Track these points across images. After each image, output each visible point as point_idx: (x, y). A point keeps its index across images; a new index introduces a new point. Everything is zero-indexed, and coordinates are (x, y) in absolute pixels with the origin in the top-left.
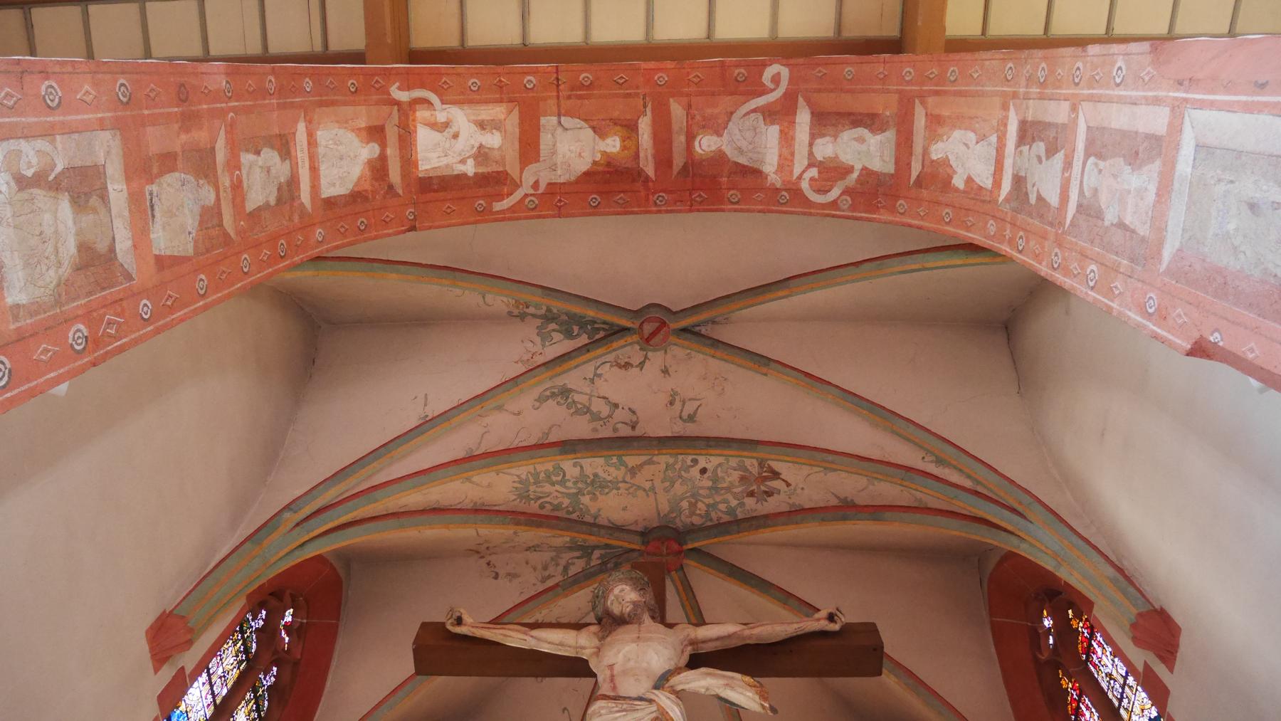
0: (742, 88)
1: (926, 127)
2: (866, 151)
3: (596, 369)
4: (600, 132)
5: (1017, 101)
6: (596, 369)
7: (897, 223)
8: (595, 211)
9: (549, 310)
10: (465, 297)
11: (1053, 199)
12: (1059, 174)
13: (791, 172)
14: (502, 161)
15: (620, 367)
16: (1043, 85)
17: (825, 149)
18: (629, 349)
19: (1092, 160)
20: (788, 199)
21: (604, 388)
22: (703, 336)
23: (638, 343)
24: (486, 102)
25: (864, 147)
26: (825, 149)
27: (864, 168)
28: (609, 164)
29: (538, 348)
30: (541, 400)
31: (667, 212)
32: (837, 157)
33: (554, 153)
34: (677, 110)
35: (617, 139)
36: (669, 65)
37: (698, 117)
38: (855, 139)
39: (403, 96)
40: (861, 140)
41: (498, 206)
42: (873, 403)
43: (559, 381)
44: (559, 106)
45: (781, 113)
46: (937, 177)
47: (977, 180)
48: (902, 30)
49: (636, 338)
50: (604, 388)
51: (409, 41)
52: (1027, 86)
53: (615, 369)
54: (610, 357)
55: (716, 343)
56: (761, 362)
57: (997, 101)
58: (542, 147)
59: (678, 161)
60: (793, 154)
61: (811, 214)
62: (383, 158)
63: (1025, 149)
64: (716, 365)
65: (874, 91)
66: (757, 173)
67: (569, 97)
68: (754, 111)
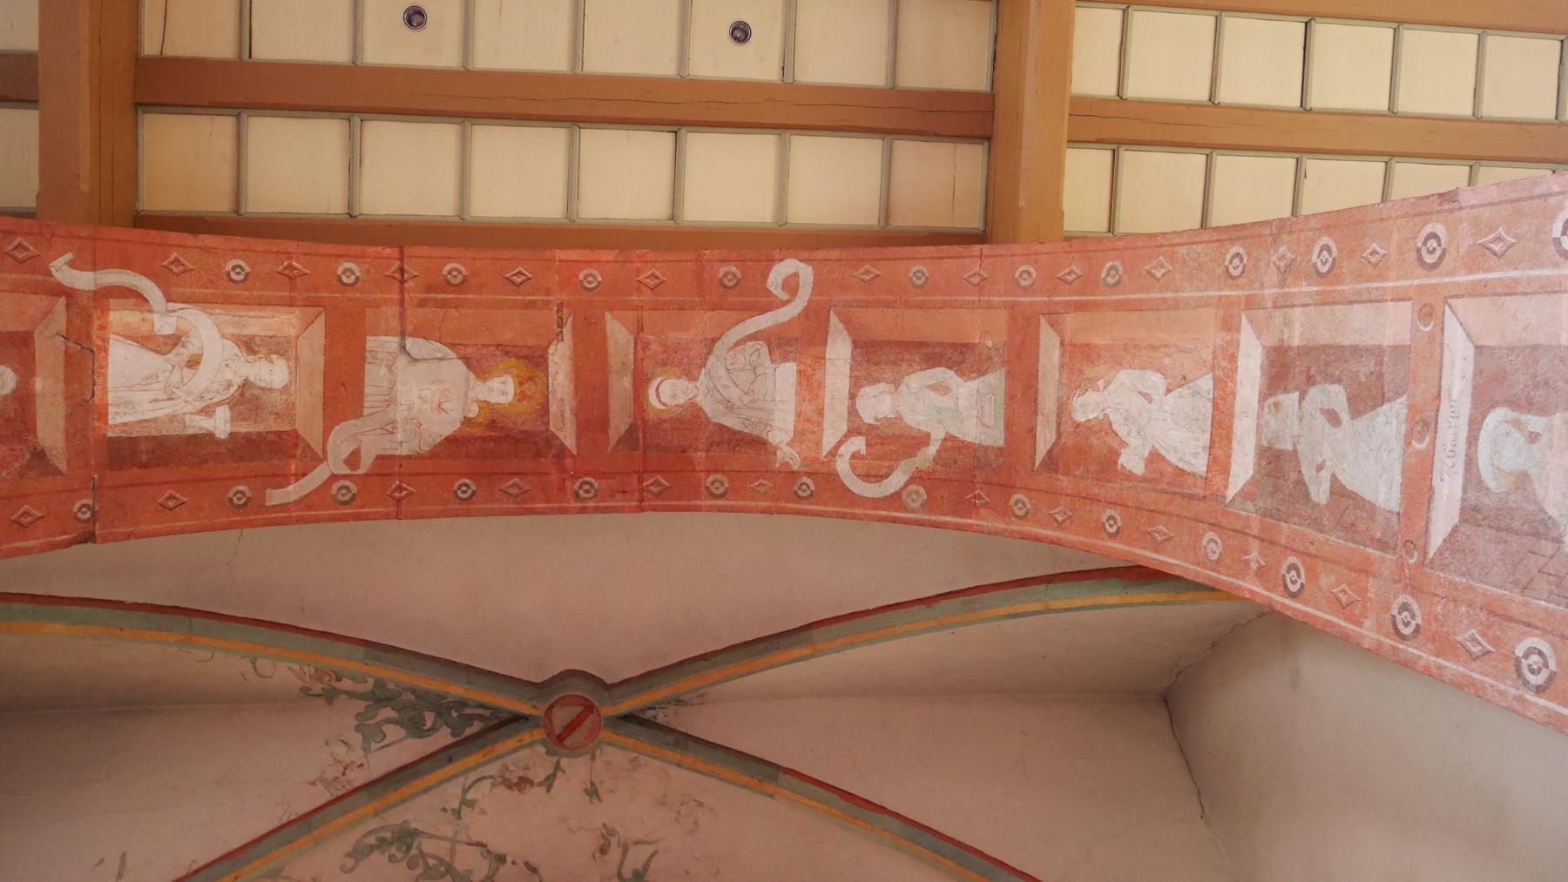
0: (732, 299)
1: (1062, 366)
2: (951, 408)
3: (465, 791)
4: (478, 367)
5: (1260, 314)
6: (465, 791)
7: (1012, 534)
8: (466, 508)
9: (380, 684)
10: (218, 662)
11: (1385, 493)
12: (1397, 446)
13: (819, 443)
14: (289, 412)
15: (510, 786)
16: (1331, 276)
17: (877, 403)
18: (526, 754)
19: (1496, 418)
20: (812, 490)
21: (478, 826)
22: (661, 727)
23: (543, 742)
24: (262, 303)
25: (947, 401)
26: (877, 403)
27: (949, 438)
28: (492, 424)
29: (357, 755)
30: (358, 853)
31: (597, 510)
32: (899, 418)
33: (391, 401)
34: (618, 333)
35: (510, 380)
36: (606, 255)
37: (654, 347)
38: (930, 387)
39: (83, 280)
40: (941, 388)
41: (276, 497)
42: (959, 844)
43: (394, 818)
44: (402, 317)
45: (800, 342)
46: (1089, 454)
47: (1173, 458)
48: (986, 223)
49: (539, 734)
50: (478, 826)
51: (136, 198)
52: (1282, 284)
53: (502, 791)
54: (493, 769)
55: (684, 741)
56: (763, 772)
57: (1210, 315)
58: (367, 390)
59: (619, 422)
60: (820, 412)
61: (854, 517)
62: (23, 397)
63: (1290, 399)
64: (683, 779)
65: (962, 305)
66: (759, 443)
67: (422, 303)
68: (753, 337)
